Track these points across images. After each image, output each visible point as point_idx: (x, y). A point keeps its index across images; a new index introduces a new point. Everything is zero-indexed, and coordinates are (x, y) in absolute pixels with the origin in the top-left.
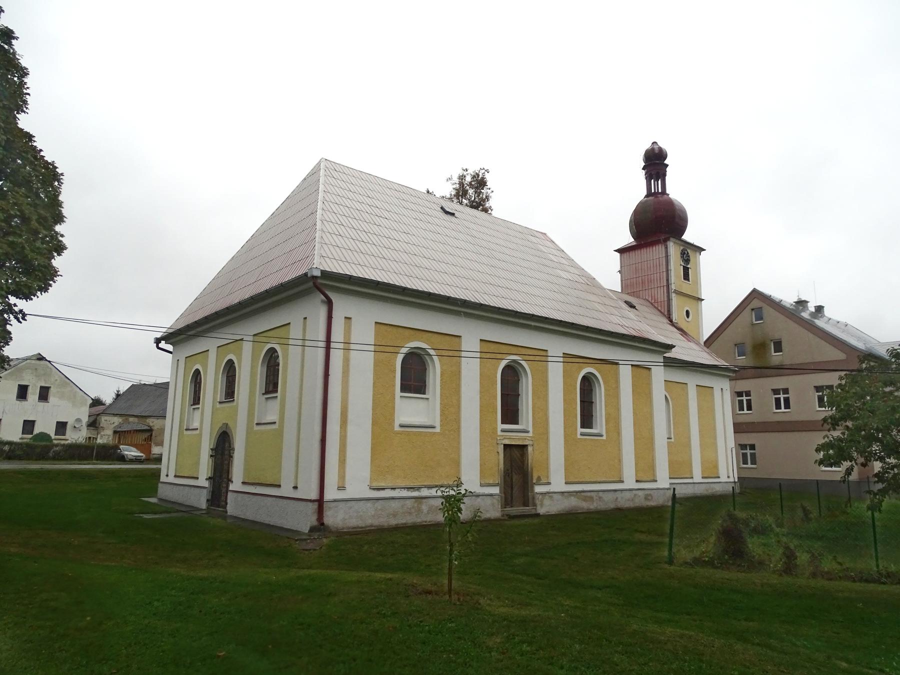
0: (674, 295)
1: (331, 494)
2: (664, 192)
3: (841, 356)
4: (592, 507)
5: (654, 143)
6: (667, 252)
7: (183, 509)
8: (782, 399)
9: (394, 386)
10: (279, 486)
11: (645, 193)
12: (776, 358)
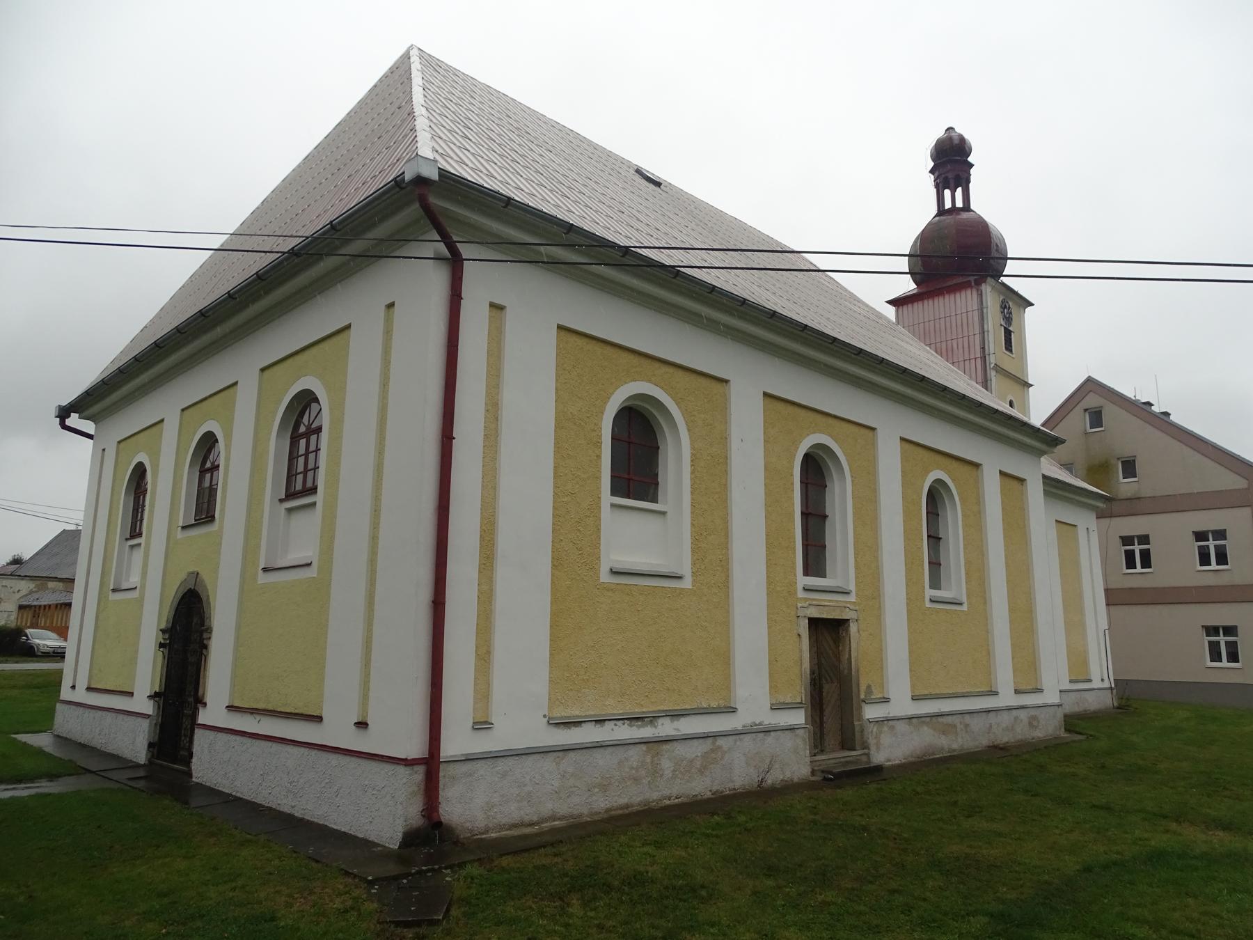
1: (457, 740)
2: (967, 207)
3: (1240, 483)
4: (955, 746)
5: (950, 129)
7: (93, 765)
9: (598, 478)
10: (319, 719)
11: (934, 211)
12: (1126, 487)
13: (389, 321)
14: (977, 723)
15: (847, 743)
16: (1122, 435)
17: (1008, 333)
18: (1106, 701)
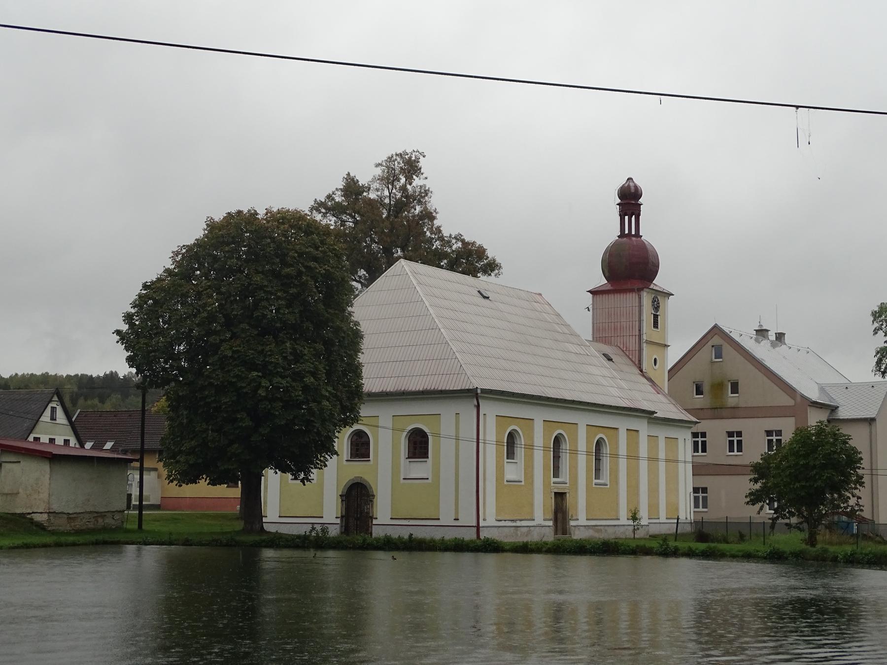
0: (645, 345)
2: (637, 235)
6: (640, 302)
8: (735, 440)
12: (732, 399)
14: (610, 530)
15: (565, 532)
17: (656, 317)
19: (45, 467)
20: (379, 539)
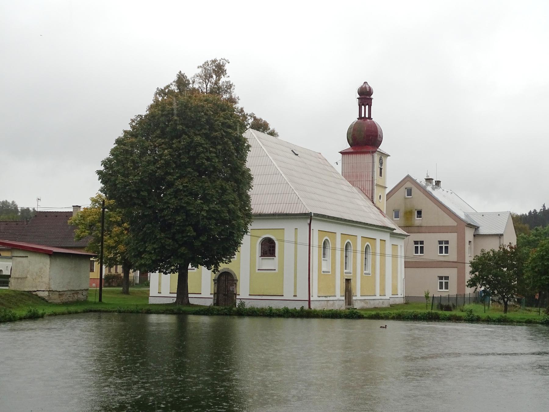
2: (370, 118)
3: (455, 224)
12: (417, 221)
13: (295, 290)
14: (372, 302)
16: (418, 200)
17: (381, 169)
18: (402, 301)
19: (46, 261)
20: (280, 310)
